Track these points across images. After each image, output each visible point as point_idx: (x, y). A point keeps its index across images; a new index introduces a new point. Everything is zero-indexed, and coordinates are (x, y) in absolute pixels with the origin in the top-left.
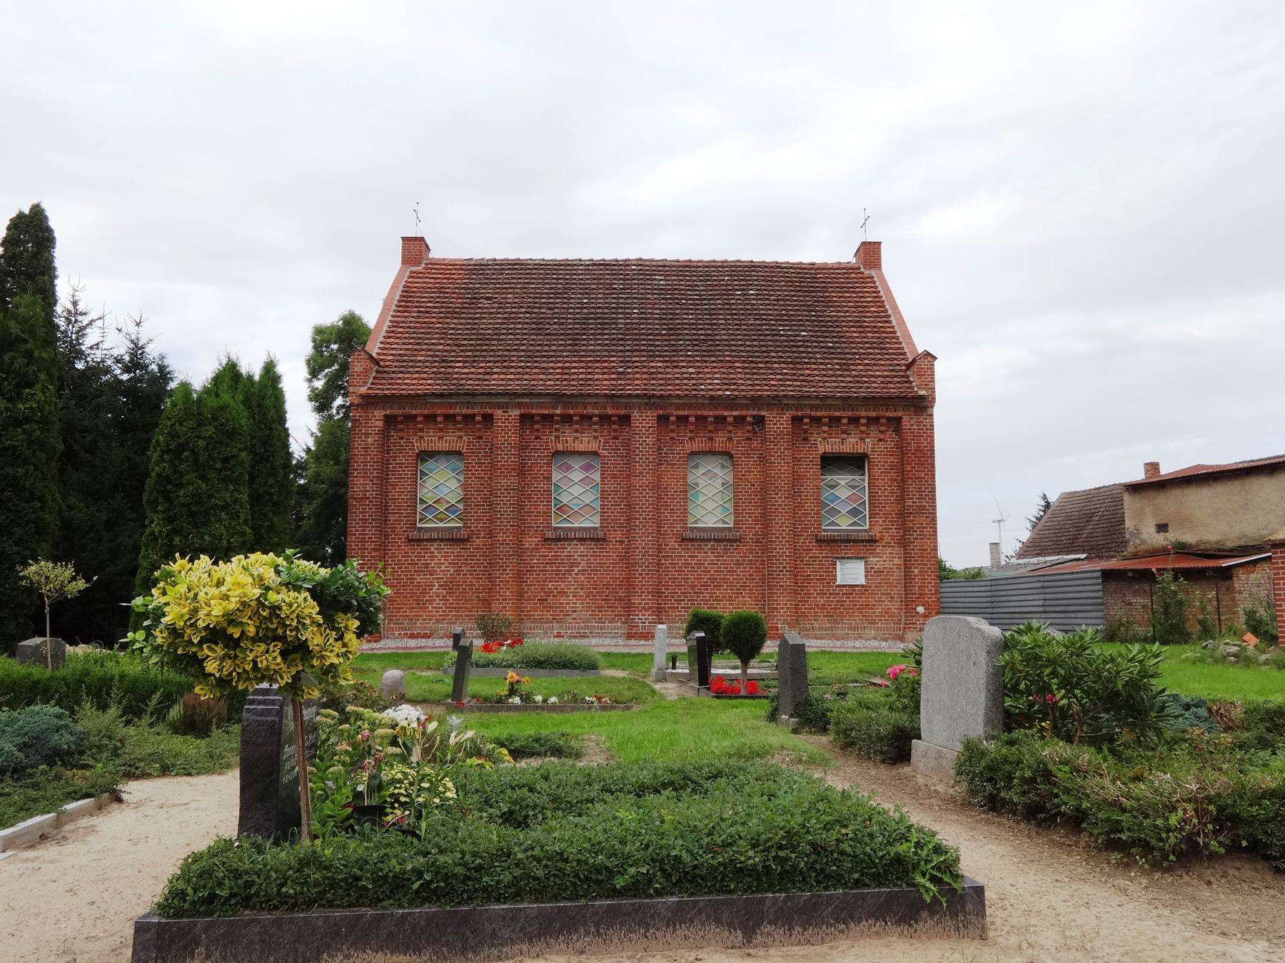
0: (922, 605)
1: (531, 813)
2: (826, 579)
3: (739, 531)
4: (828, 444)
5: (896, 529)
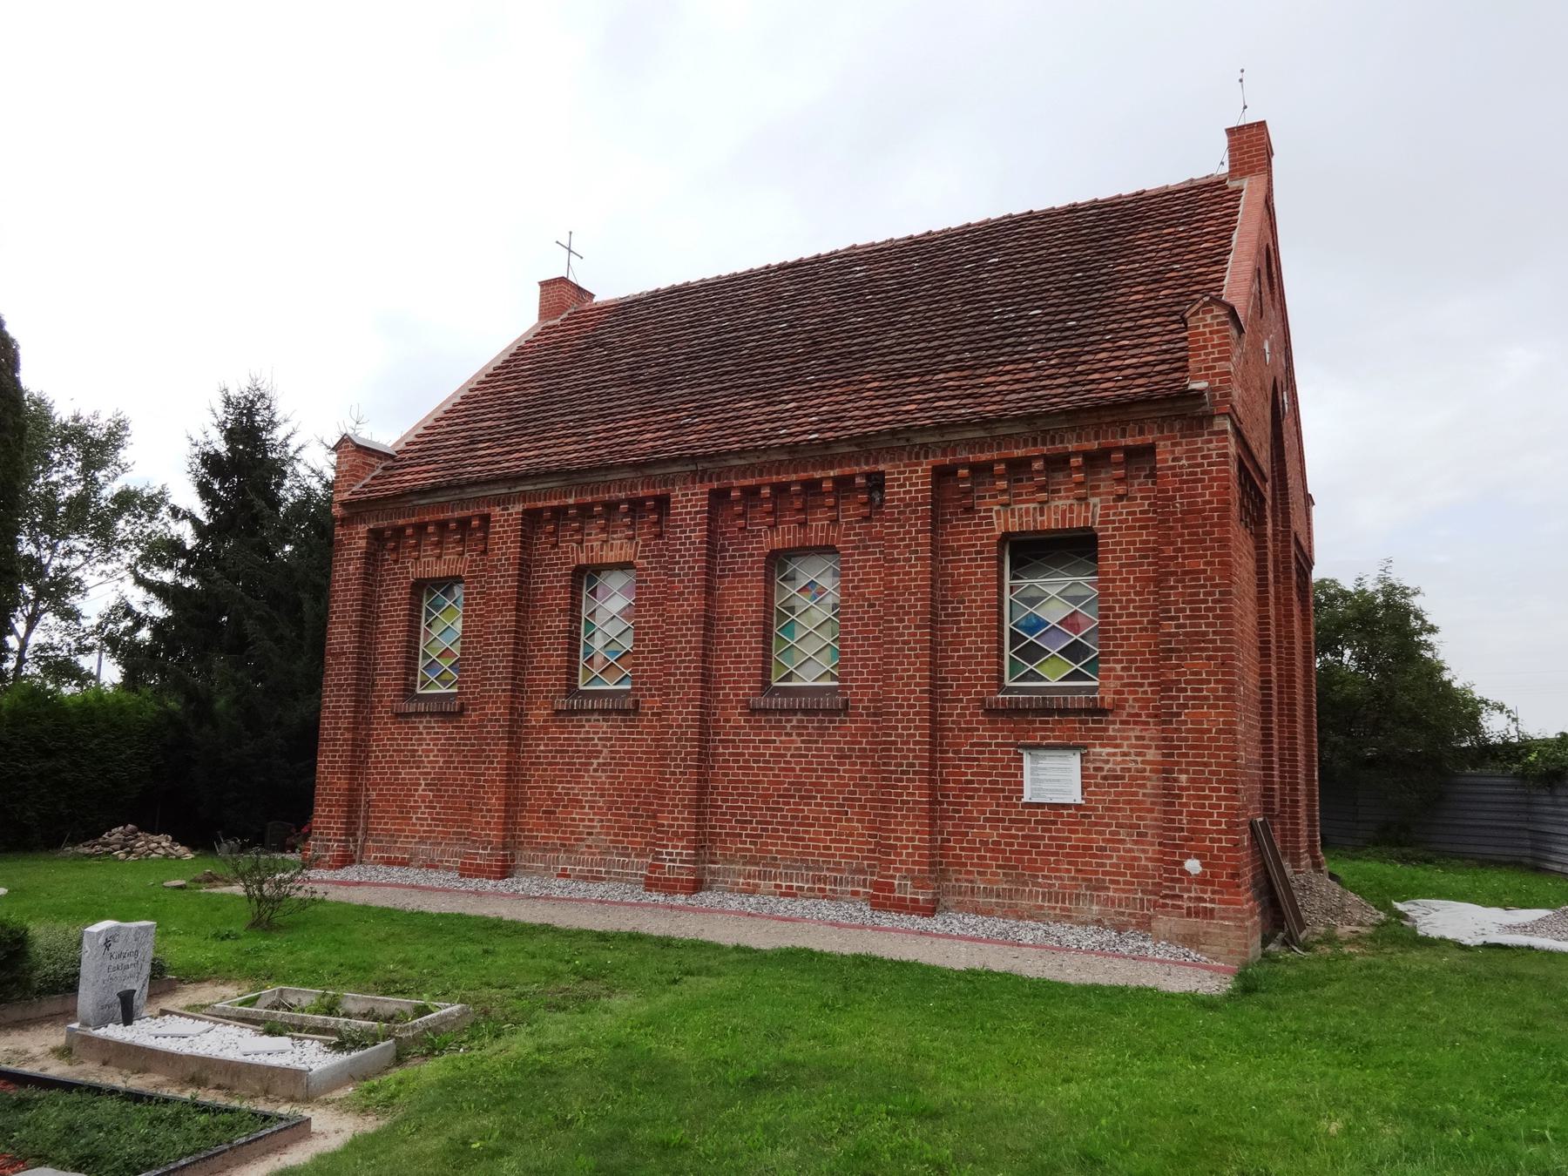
0: (1197, 857)
2: (1003, 791)
4: (1013, 515)
5: (1151, 685)
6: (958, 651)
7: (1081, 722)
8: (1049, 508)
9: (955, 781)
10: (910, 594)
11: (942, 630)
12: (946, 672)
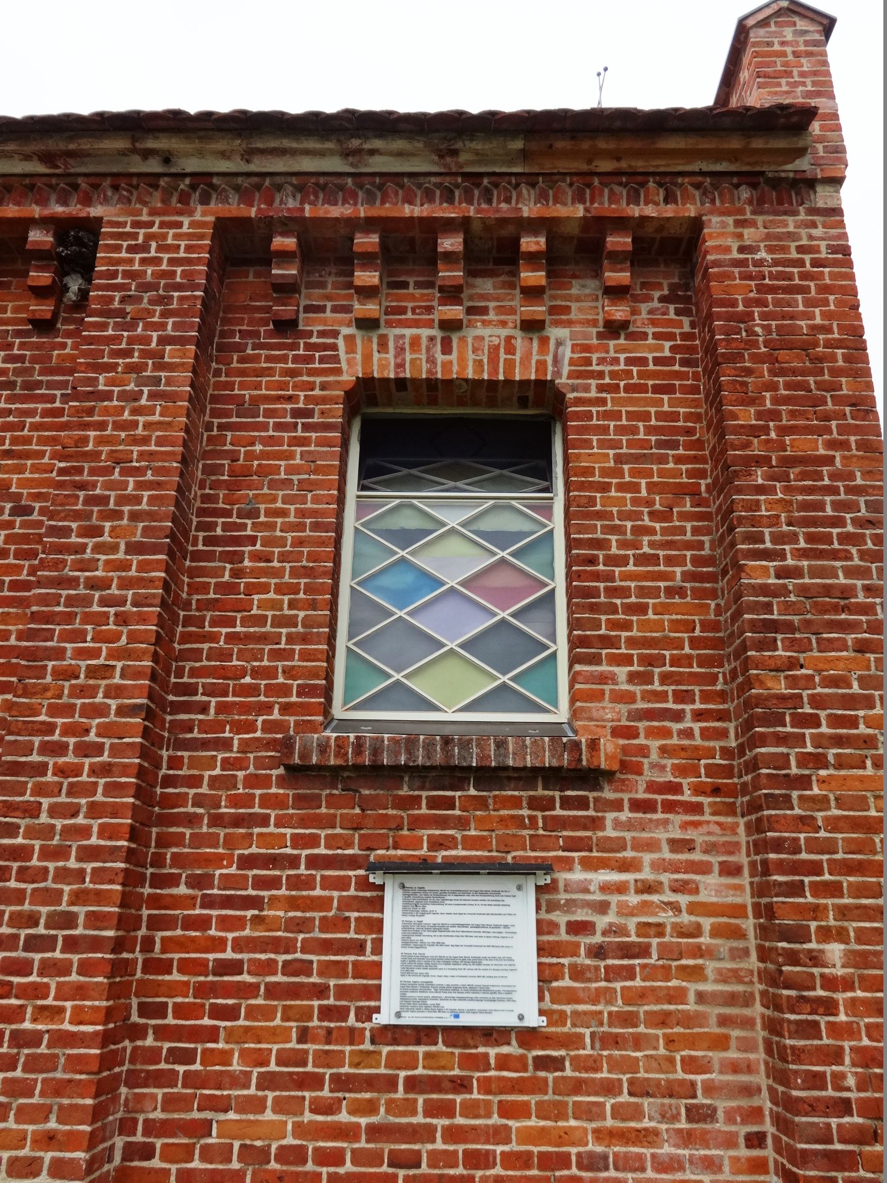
2: (321, 991)
4: (383, 345)
5: (699, 715)
6: (231, 623)
7: (535, 803)
8: (463, 339)
9: (186, 967)
10: (125, 472)
11: (192, 573)
12: (194, 673)
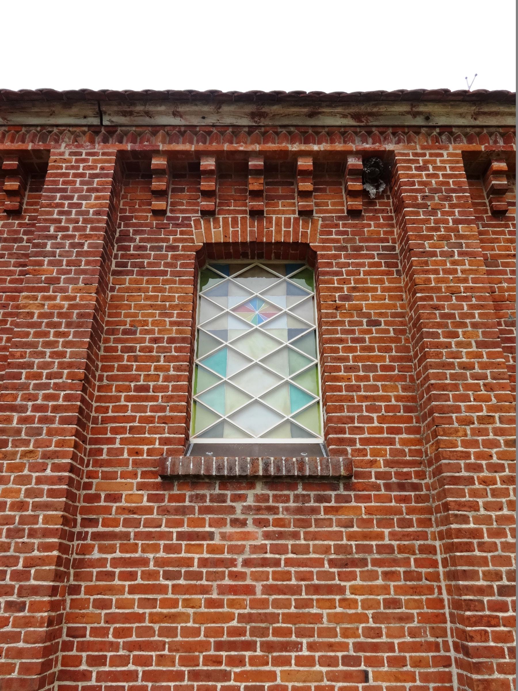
1: (259, 586)
3: (344, 452)
